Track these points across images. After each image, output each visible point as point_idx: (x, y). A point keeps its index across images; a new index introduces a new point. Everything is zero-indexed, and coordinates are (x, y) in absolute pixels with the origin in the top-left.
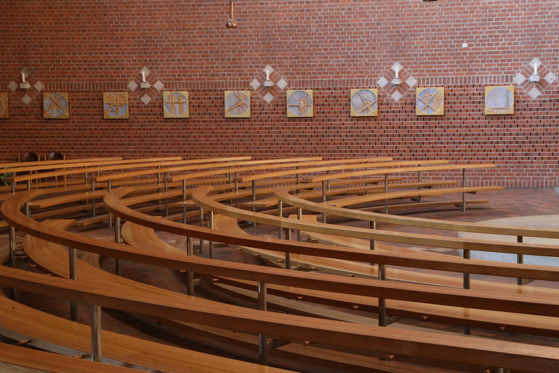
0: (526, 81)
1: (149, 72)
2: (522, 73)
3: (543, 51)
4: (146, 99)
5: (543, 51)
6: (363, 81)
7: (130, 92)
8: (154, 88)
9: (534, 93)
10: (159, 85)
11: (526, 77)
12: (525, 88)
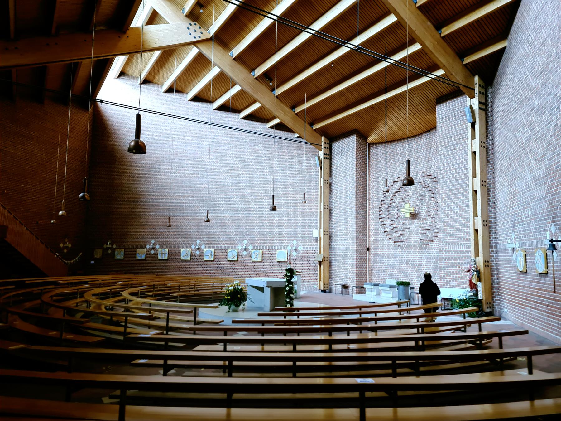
2: (290, 246)
4: (152, 252)
5: (297, 238)
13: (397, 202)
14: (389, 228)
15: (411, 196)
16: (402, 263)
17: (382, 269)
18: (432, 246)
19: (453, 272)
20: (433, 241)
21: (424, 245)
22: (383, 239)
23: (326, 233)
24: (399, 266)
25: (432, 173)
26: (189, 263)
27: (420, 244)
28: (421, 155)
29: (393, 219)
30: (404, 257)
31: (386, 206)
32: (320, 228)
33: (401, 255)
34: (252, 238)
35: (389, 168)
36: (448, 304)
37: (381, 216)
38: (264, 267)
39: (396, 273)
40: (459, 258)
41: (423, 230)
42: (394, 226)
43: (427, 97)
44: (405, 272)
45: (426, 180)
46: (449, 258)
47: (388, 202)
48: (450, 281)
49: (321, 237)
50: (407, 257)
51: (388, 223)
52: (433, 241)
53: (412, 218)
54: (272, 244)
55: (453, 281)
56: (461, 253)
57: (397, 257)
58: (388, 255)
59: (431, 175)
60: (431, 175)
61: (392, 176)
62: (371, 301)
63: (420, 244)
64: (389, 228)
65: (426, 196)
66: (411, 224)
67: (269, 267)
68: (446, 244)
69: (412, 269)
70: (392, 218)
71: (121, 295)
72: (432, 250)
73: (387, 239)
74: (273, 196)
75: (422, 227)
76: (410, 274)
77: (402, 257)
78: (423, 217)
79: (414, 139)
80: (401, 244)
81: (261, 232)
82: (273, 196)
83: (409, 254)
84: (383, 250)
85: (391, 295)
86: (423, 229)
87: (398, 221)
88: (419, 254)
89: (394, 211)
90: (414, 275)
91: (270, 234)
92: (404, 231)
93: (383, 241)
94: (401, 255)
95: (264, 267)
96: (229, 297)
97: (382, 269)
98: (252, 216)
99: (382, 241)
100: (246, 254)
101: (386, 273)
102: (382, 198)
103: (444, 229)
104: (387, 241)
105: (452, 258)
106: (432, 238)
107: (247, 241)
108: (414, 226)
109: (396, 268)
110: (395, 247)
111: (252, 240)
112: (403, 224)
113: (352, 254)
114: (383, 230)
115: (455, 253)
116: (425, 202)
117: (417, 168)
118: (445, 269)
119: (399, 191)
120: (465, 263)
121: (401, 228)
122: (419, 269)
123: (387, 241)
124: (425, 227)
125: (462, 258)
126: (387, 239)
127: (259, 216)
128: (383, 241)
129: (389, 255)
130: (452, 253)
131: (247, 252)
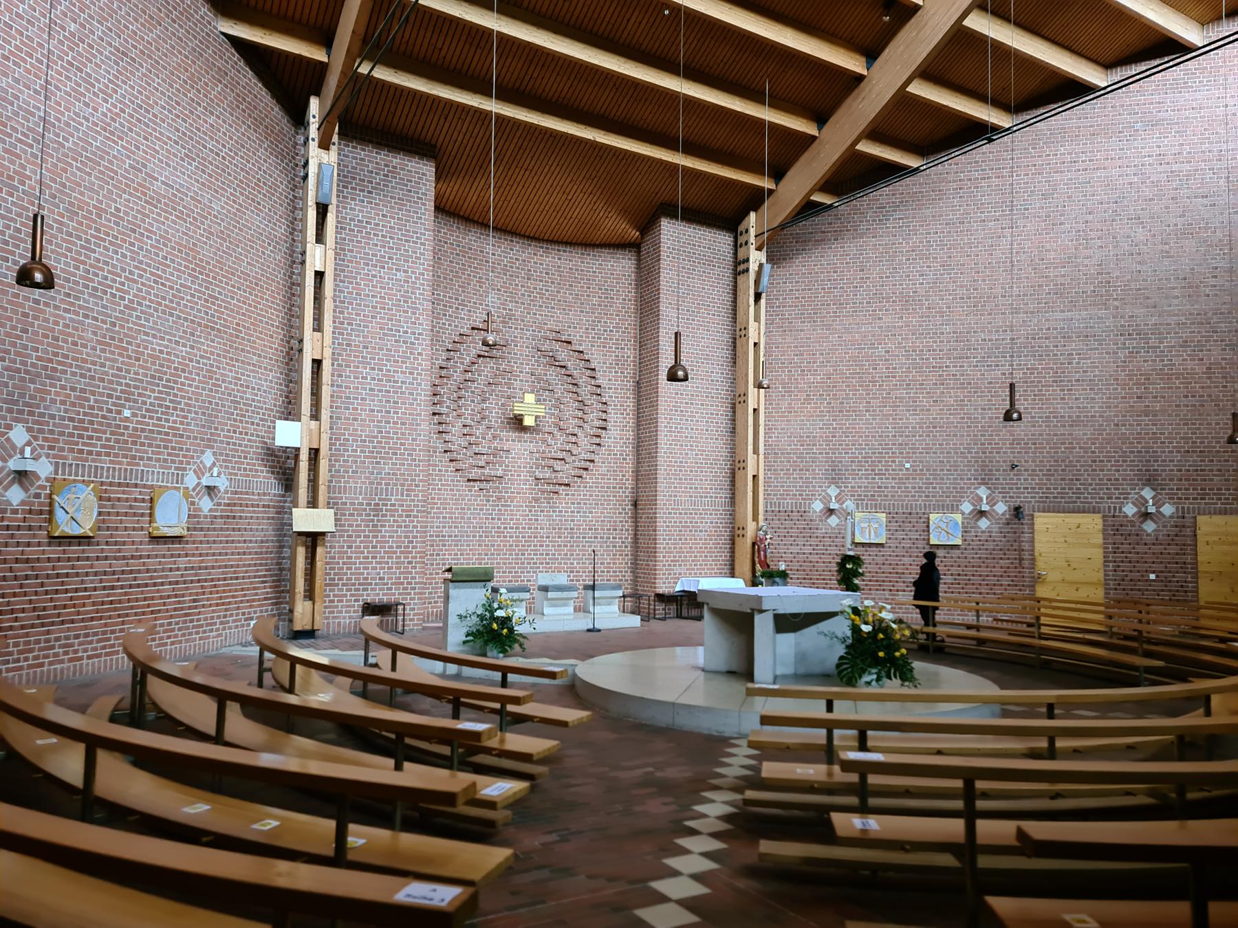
0: (198, 484)
1: (989, 492)
3: (215, 441)
4: (833, 521)
6: (943, 506)
7: (963, 514)
8: (994, 510)
9: (206, 504)
10: (849, 505)
11: (199, 478)
12: (197, 494)
13: (482, 380)
14: (458, 442)
15: (517, 376)
16: (486, 532)
17: (434, 550)
18: (567, 495)
19: (681, 548)
20: (568, 485)
21: (543, 492)
22: (440, 470)
23: (742, 465)
24: (479, 541)
25: (574, 340)
26: (956, 552)
27: (534, 489)
28: (547, 290)
29: (469, 422)
30: (493, 519)
31: (452, 385)
32: (315, 416)
33: (484, 514)
34: (53, 417)
35: (462, 287)
36: (669, 609)
37: (438, 409)
38: (101, 566)
39: (469, 559)
40: (691, 522)
41: (543, 459)
42: (473, 439)
43: (521, 151)
44: (493, 554)
45: (558, 351)
46: (675, 522)
47: (457, 376)
48: (675, 565)
49: (315, 453)
50: (499, 519)
51: (456, 429)
52: (568, 485)
53: (517, 428)
54: (134, 457)
55: (680, 565)
56: (696, 514)
57: (474, 518)
58: (451, 513)
59: (570, 343)
60: (570, 343)
61: (470, 311)
62: (591, 627)
63: (534, 489)
64: (457, 441)
65: (557, 384)
66: (513, 441)
67: (118, 565)
68: (671, 496)
69: (511, 546)
70: (467, 419)
71: (559, 836)
72: (567, 503)
73: (451, 471)
74: (1012, 386)
75: (544, 452)
76: (506, 559)
77: (487, 519)
78: (547, 429)
79: (530, 245)
80: (484, 485)
81: (93, 393)
82: (1012, 386)
83: (506, 510)
84: (439, 499)
85: (571, 609)
86: (544, 455)
87: (482, 428)
88: (530, 511)
89: (473, 401)
90: (517, 559)
91: (127, 413)
92: (495, 455)
93: (441, 475)
94: (484, 514)
95: (101, 566)
96: (897, 654)
97: (434, 550)
98: (56, 307)
99: (436, 475)
100: (23, 503)
101: (443, 559)
102: (443, 360)
103: (668, 466)
104: (451, 476)
105: (681, 522)
106: (567, 478)
107: (29, 430)
108: (520, 449)
109: (469, 545)
110: (470, 494)
111: (51, 432)
112: (494, 437)
113: (413, 511)
114: (441, 447)
115: (686, 514)
116: (552, 397)
117: (535, 314)
118: (668, 544)
119: (486, 354)
120: (701, 531)
121: (489, 448)
122: (530, 546)
123: (451, 476)
124: (550, 452)
125: (697, 522)
126: (451, 471)
127: (86, 316)
128: (441, 475)
129: (455, 513)
130: (680, 514)
131: (26, 490)
